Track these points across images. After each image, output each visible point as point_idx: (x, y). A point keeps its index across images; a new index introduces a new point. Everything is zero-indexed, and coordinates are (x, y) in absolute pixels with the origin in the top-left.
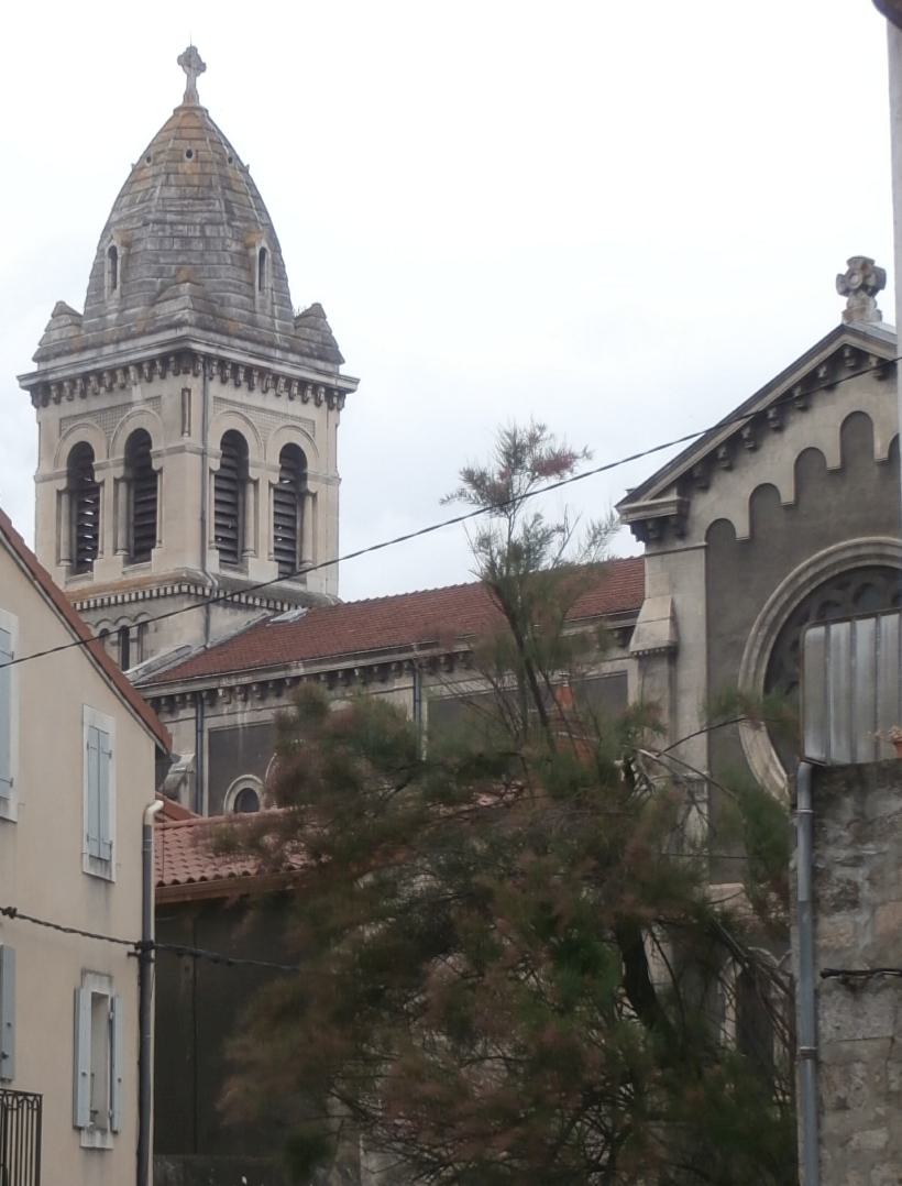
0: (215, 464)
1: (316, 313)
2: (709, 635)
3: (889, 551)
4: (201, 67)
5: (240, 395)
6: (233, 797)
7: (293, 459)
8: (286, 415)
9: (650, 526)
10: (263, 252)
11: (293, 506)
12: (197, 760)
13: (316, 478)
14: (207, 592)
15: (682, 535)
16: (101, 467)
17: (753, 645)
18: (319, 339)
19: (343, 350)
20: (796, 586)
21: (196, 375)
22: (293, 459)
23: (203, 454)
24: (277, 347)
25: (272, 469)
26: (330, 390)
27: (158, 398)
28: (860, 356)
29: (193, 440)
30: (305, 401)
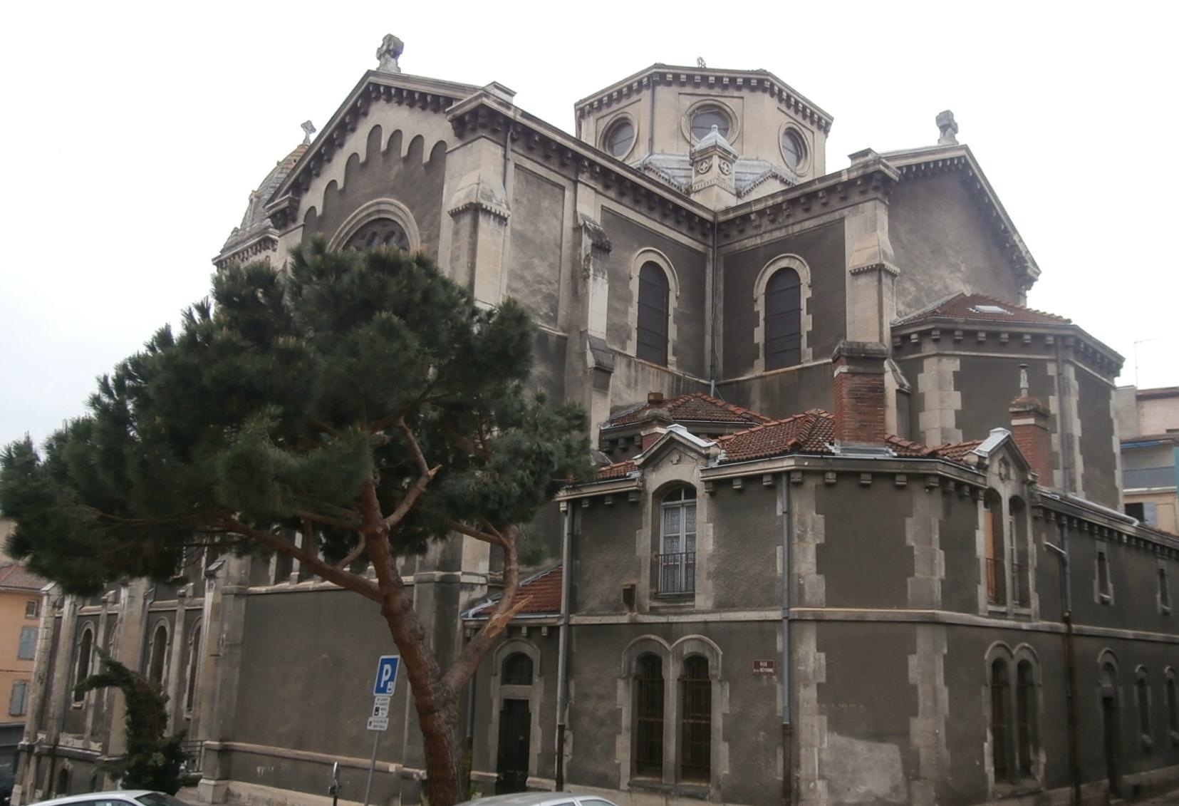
9: (278, 216)
15: (294, 220)
20: (339, 239)
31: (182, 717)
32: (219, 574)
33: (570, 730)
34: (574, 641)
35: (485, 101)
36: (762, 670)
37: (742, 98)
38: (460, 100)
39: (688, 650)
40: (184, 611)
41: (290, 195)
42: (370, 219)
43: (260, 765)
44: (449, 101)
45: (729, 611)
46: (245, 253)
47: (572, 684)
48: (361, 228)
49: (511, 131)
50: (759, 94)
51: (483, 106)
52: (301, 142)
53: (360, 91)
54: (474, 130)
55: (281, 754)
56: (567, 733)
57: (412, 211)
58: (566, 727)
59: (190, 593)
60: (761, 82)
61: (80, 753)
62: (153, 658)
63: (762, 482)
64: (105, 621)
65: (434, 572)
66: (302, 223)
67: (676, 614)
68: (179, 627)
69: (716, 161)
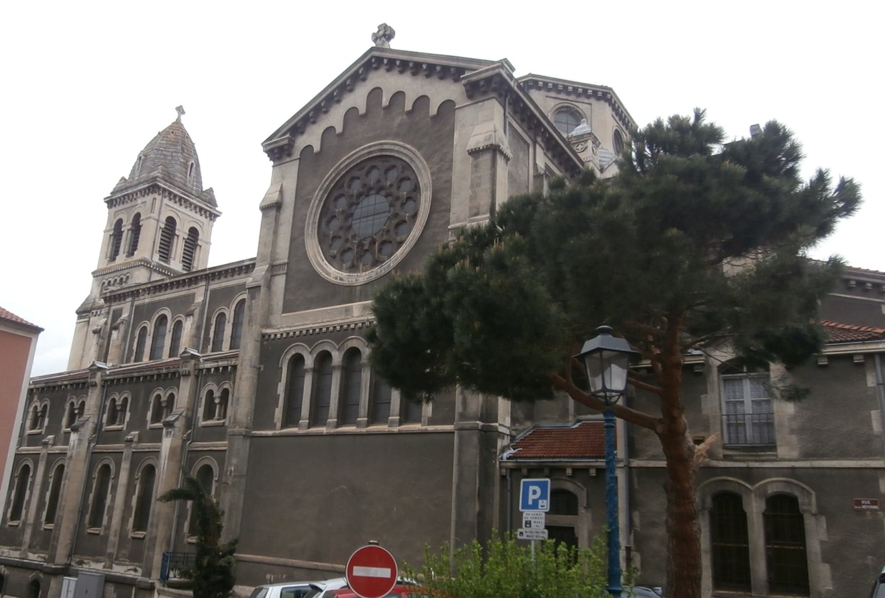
0: (163, 226)
1: (211, 190)
2: (296, 198)
3: (385, 147)
4: (183, 113)
5: (177, 206)
6: (139, 329)
7: (193, 232)
8: (193, 218)
9: (276, 151)
10: (192, 164)
11: (192, 249)
12: (129, 316)
13: (202, 240)
14: (152, 267)
15: (289, 155)
16: (124, 226)
17: (316, 199)
18: (210, 197)
19: (218, 203)
20: (338, 170)
21: (159, 194)
22: (193, 232)
23: (158, 221)
24: (193, 195)
25: (185, 233)
26: (211, 214)
27: (145, 202)
28: (380, 60)
29: (155, 215)
30: (201, 215)
31: (127, 536)
32: (177, 424)
33: (637, 551)
34: (636, 480)
36: (864, 507)
37: (590, 104)
38: (475, 70)
39: (771, 490)
40: (131, 453)
41: (288, 135)
42: (371, 156)
43: (270, 573)
44: (461, 70)
45: (819, 460)
46: (135, 194)
47: (636, 514)
48: (361, 162)
49: (509, 97)
50: (602, 102)
51: (499, 75)
52: (175, 121)
53: (363, 62)
54: (485, 93)
55: (296, 565)
56: (633, 553)
57: (419, 150)
58: (632, 549)
59: (136, 439)
60: (605, 94)
61: (18, 562)
62: (96, 489)
63: (853, 360)
64: (45, 459)
65: (478, 422)
66: (299, 157)
67: (756, 461)
68: (125, 466)
69: (590, 144)
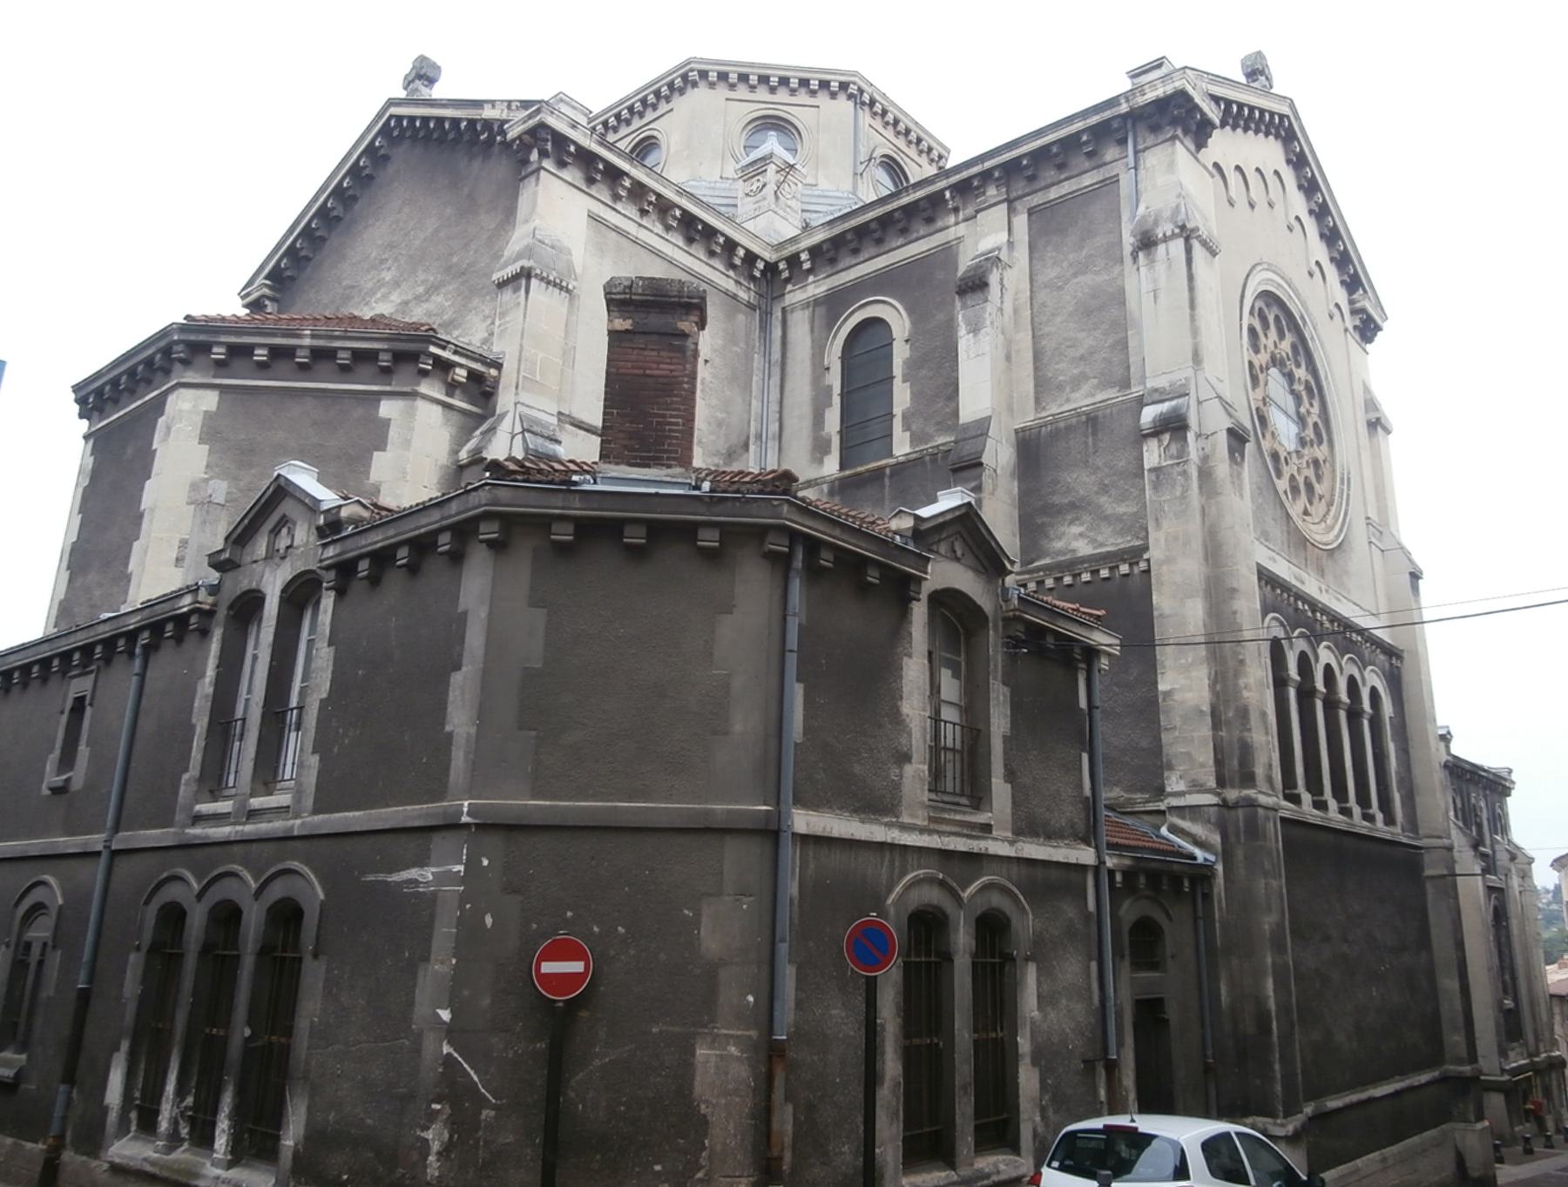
35: (552, 121)
